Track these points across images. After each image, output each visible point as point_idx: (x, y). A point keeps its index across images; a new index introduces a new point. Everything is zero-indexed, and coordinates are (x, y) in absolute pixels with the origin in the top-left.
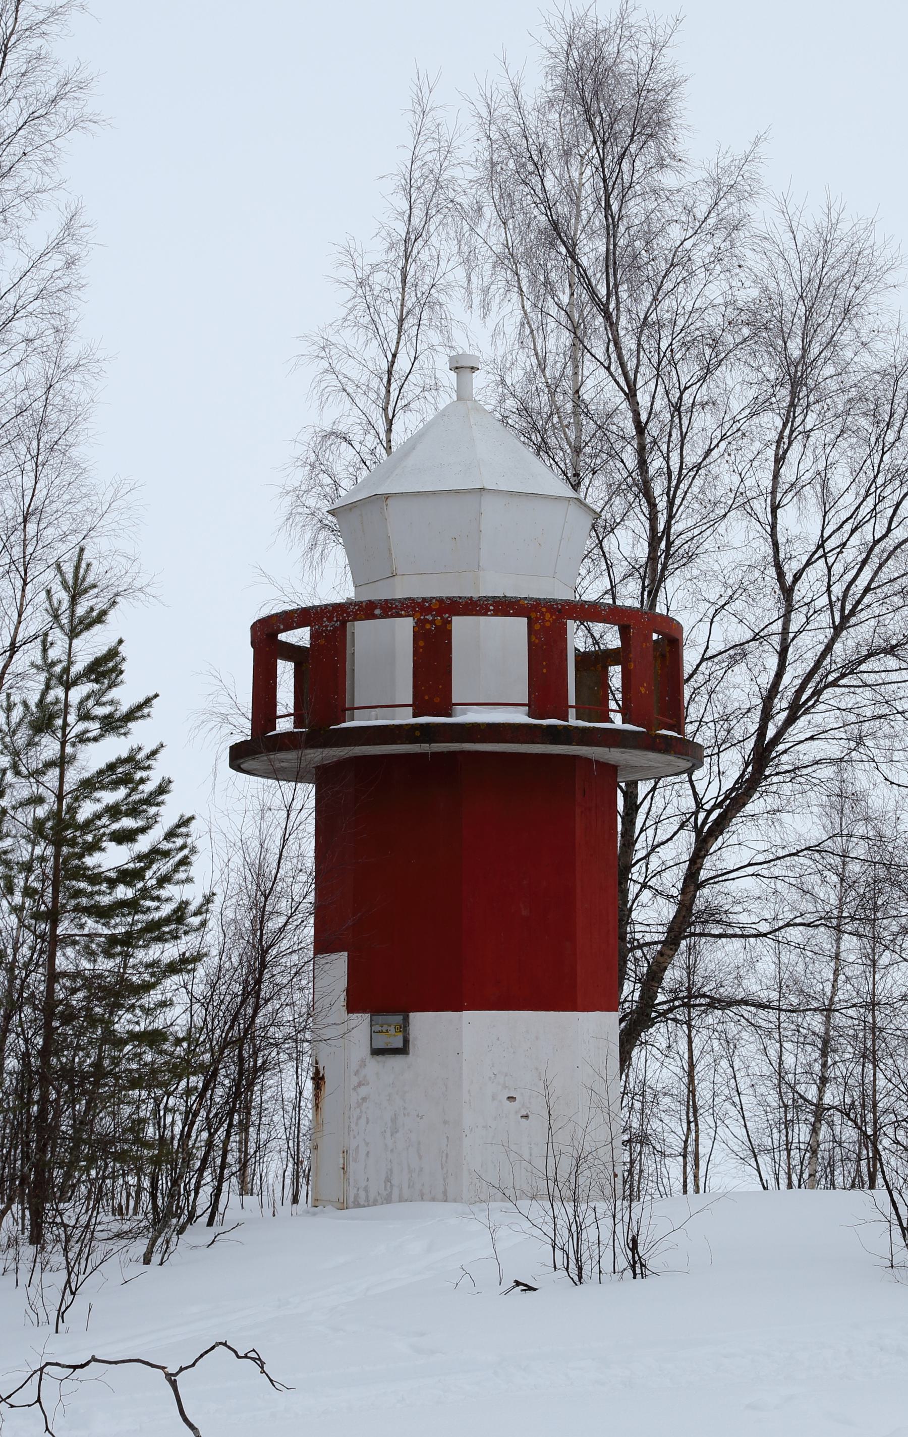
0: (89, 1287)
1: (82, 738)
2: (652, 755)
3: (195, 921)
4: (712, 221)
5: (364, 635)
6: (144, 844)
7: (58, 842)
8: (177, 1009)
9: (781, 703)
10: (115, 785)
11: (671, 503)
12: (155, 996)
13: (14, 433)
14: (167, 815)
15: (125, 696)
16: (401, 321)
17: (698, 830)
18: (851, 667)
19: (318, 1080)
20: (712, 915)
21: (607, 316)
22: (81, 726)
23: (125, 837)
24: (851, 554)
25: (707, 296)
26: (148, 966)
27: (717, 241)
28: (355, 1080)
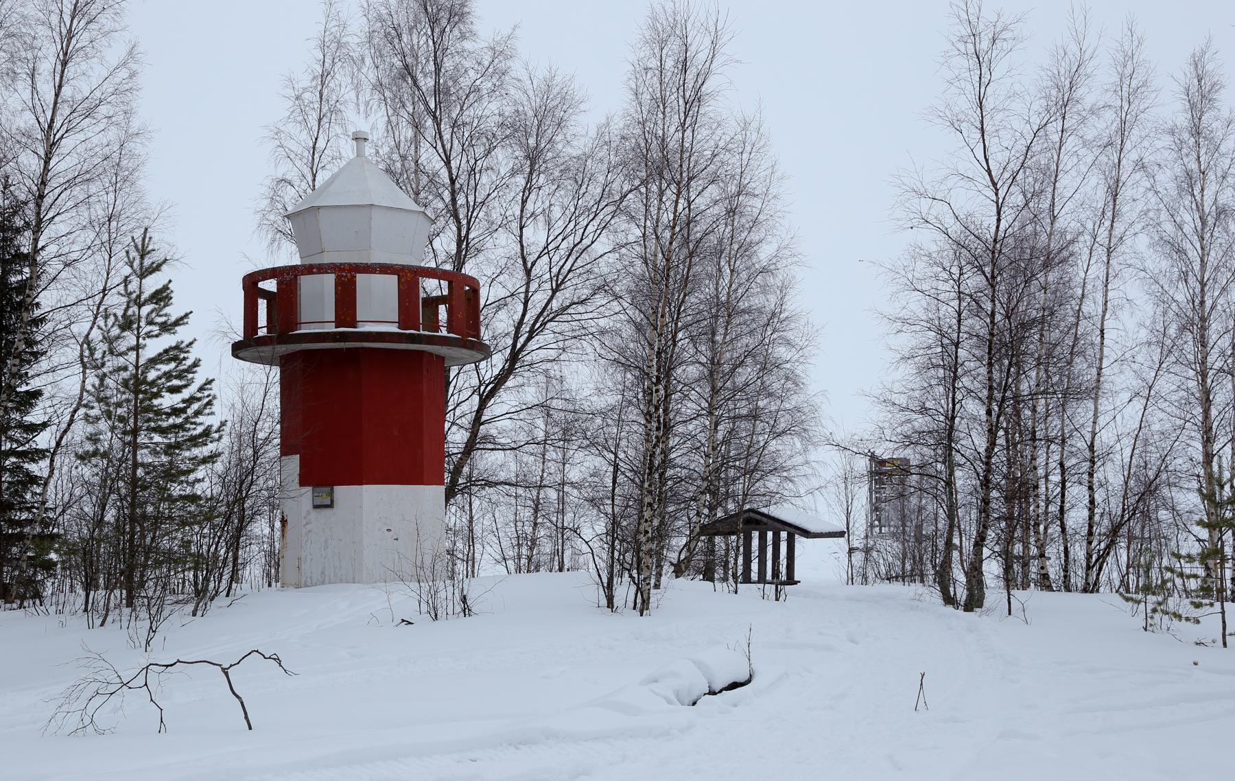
0: (163, 628)
1: (149, 335)
2: (465, 351)
3: (216, 436)
4: (490, 70)
5: (307, 284)
6: (186, 394)
7: (136, 392)
8: (206, 482)
9: (526, 329)
10: (170, 360)
11: (469, 223)
12: (192, 477)
13: (101, 170)
14: (199, 378)
15: (173, 312)
16: (320, 120)
17: (481, 396)
18: (563, 310)
19: (284, 522)
20: (487, 438)
21: (435, 117)
22: (149, 328)
23: (175, 390)
24: (563, 251)
25: (489, 112)
26: (190, 459)
27: (494, 80)
28: (304, 522)
